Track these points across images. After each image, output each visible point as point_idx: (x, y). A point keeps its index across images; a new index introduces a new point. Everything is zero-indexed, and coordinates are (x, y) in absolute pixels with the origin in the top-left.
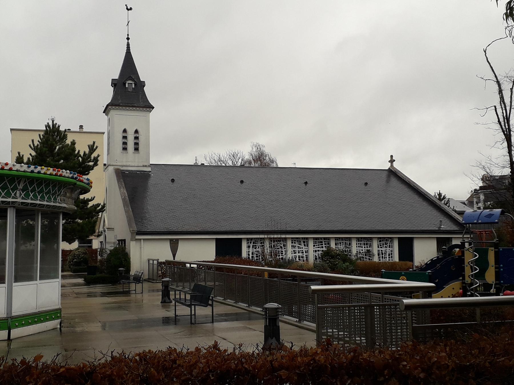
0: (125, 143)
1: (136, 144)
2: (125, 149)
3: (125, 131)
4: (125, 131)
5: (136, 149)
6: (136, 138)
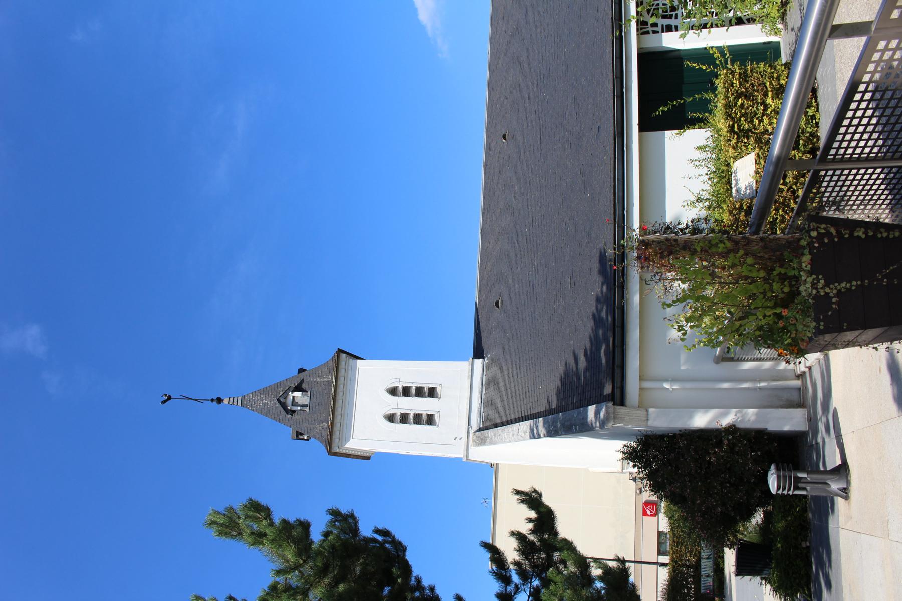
0: (418, 419)
1: (420, 392)
3: (391, 418)
4: (391, 418)
6: (406, 392)
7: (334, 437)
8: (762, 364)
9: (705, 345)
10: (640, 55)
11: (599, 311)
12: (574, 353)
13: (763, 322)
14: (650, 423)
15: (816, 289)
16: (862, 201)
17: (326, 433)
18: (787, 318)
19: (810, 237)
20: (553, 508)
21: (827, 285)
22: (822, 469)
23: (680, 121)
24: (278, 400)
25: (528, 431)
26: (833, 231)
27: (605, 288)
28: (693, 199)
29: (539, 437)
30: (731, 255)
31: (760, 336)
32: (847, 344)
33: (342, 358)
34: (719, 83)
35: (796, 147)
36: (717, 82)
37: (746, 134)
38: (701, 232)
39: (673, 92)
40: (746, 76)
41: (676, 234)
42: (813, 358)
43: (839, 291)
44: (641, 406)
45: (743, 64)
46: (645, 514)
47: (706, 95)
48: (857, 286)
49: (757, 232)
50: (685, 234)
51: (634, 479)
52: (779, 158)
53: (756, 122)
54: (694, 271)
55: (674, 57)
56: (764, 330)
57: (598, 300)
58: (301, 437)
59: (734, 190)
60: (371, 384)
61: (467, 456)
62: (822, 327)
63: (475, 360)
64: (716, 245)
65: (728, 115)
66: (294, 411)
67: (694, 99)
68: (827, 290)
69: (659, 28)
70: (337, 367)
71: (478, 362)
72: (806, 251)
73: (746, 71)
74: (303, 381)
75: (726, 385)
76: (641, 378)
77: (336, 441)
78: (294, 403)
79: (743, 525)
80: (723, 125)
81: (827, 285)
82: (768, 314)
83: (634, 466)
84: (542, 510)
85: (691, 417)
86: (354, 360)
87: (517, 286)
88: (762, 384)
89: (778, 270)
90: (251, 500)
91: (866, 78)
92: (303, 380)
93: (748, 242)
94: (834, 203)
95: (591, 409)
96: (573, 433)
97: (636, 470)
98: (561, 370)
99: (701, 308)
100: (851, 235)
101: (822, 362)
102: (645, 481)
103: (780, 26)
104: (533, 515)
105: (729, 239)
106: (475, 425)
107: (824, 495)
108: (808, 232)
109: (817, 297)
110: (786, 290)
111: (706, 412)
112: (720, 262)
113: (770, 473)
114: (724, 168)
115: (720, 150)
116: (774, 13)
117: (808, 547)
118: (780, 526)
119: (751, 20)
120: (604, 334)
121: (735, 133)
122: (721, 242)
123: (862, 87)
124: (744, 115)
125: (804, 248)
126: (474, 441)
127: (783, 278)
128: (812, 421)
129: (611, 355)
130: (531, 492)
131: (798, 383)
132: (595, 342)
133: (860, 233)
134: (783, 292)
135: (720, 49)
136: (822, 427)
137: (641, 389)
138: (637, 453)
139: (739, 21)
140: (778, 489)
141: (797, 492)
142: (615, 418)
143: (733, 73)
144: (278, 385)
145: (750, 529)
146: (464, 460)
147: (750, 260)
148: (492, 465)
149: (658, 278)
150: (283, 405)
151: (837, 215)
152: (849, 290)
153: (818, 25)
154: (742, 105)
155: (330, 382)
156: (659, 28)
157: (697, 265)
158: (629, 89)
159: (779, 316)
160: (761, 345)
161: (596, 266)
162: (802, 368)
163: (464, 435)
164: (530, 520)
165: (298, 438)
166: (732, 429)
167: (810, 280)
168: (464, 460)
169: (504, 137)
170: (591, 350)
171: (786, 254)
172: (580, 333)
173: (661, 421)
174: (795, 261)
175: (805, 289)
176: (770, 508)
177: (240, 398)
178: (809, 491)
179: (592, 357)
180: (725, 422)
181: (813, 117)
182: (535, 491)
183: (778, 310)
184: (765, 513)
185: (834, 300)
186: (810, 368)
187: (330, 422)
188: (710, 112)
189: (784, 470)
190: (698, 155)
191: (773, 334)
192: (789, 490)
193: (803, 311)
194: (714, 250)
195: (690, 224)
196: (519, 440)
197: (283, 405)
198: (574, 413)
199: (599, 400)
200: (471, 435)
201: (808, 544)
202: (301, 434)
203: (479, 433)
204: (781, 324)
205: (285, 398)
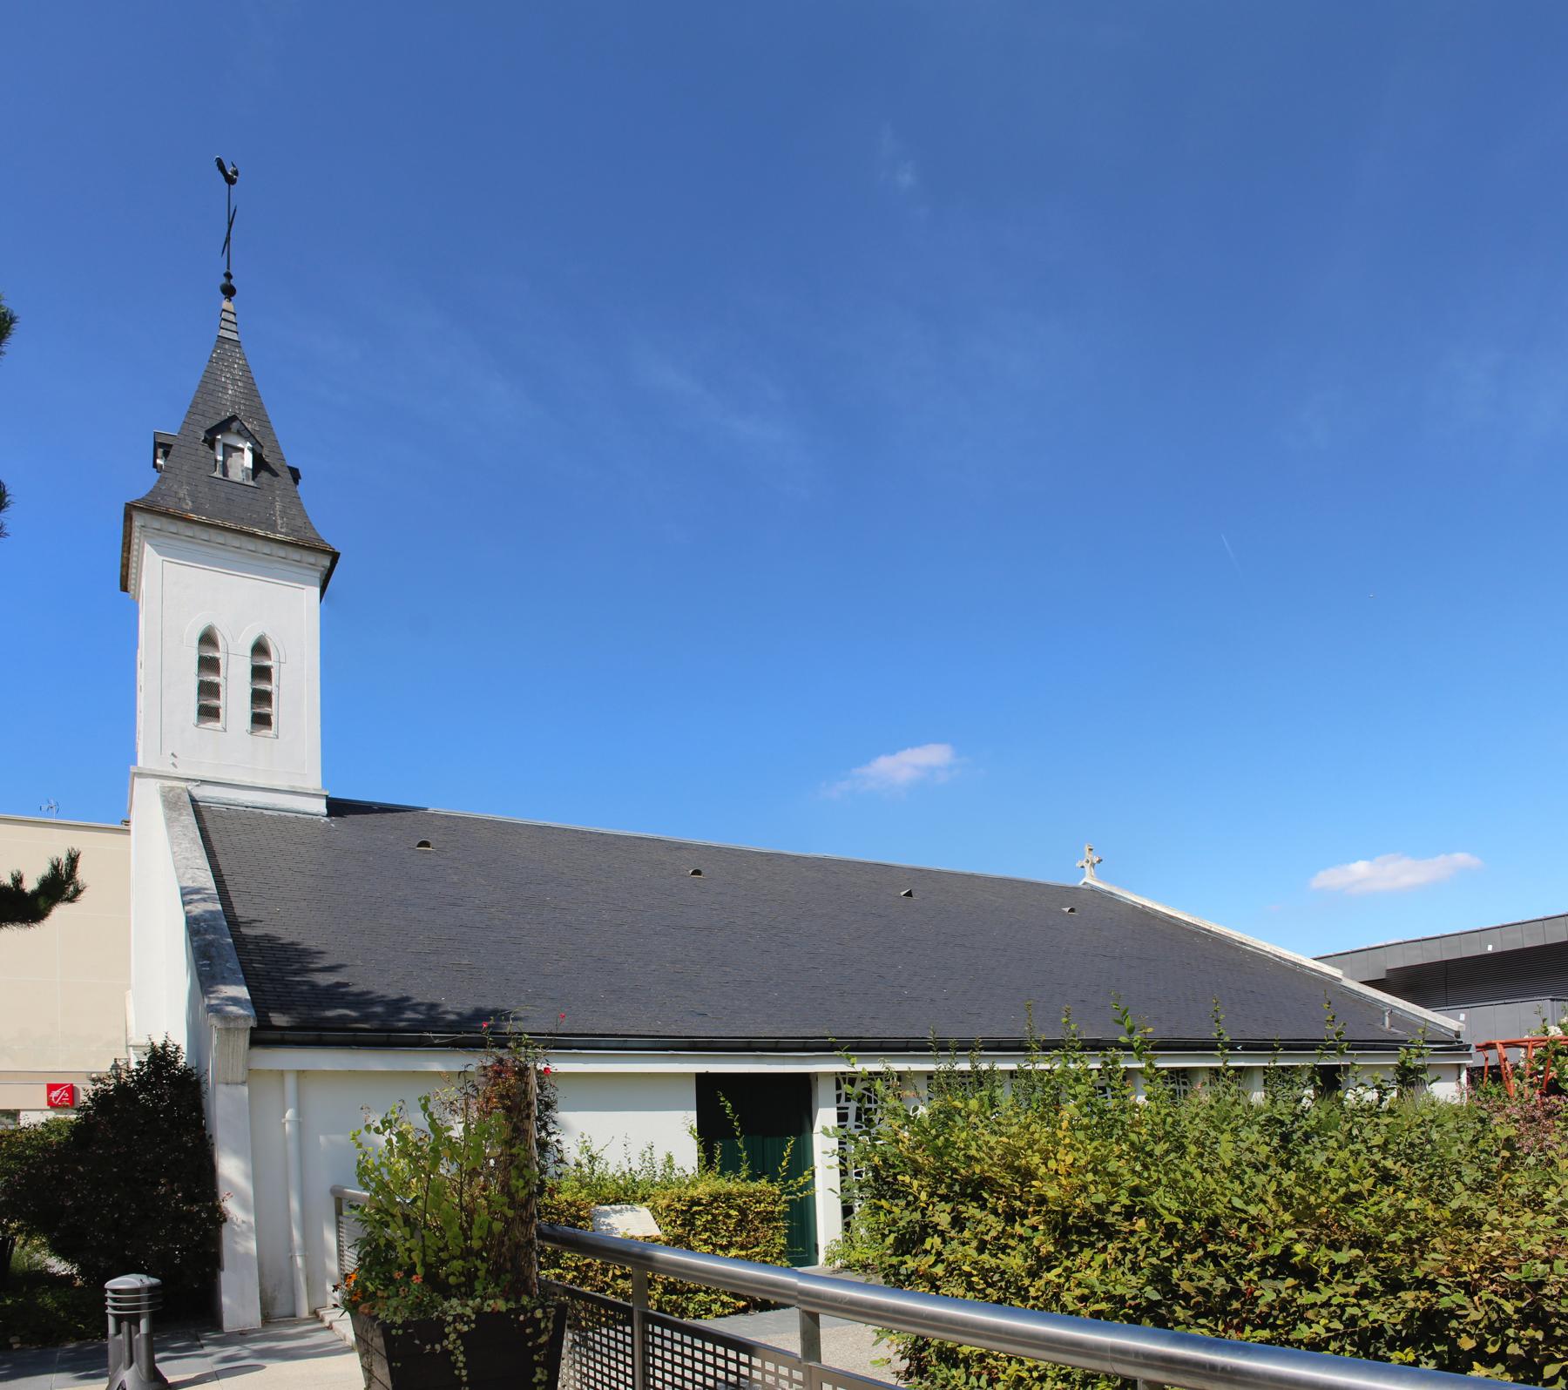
0: (208, 690)
1: (261, 697)
2: (208, 713)
3: (208, 639)
4: (208, 639)
5: (261, 720)
6: (261, 673)
7: (164, 520)
8: (334, 1254)
9: (359, 1162)
10: (806, 1078)
11: (414, 1008)
12: (341, 966)
13: (400, 1249)
14: (222, 1088)
15: (454, 1321)
16: (587, 1375)
17: (170, 504)
18: (408, 1284)
19: (535, 1309)
20: (47, 922)
21: (461, 1335)
22: (157, 1356)
23: (710, 1131)
24: (234, 418)
25: (196, 885)
26: (544, 1339)
27: (452, 1017)
28: (594, 1150)
29: (184, 904)
30: (505, 1199)
31: (378, 1245)
32: (368, 1370)
33: (327, 565)
34: (762, 1184)
35: (670, 1289)
36: (763, 1181)
37: (689, 1223)
38: (542, 1155)
39: (751, 1122)
40: (769, 1221)
41: (539, 1119)
42: (345, 1327)
43: (452, 1353)
44: (252, 1075)
45: (786, 1216)
46: (51, 1088)
47: (745, 1167)
48: (460, 1376)
49: (541, 1235)
50: (539, 1131)
51: (115, 1067)
52: (650, 1259)
53: (705, 1236)
54: (480, 1145)
55: (801, 1122)
56: (386, 1251)
57: (433, 1006)
58: (160, 451)
59: (606, 1208)
60: (277, 609)
61: (141, 775)
62: (394, 1332)
63: (324, 802)
64: (521, 1176)
65: (715, 1198)
66: (212, 446)
67: (740, 1151)
68: (453, 1337)
69: (843, 1103)
70: (303, 547)
71: (320, 807)
72: (512, 1305)
73: (776, 1220)
74: (275, 474)
75: (295, 1205)
76: (300, 1074)
77: (157, 522)
78: (229, 450)
79: (43, 1244)
80: (702, 1191)
81: (461, 1335)
82: (413, 1255)
83: (139, 1063)
84: (42, 902)
85: (236, 1152)
86: (318, 582)
87: (455, 879)
88: (299, 1261)
89: (483, 1267)
90: (12, 320)
91: (756, 1362)
92: (276, 475)
93: (526, 1223)
94: (586, 1338)
95: (242, 992)
96: (196, 962)
97: (134, 1066)
98: (310, 943)
99: (425, 1153)
100: (538, 1364)
101: (341, 1345)
102: (113, 1081)
103: (838, 1263)
104: (30, 885)
105: (531, 1195)
106: (201, 792)
107: (111, 1361)
108: (542, 1306)
109: (441, 1322)
110: (452, 1280)
111: (247, 1177)
112: (494, 1189)
113: (144, 1277)
114: (639, 1195)
115: (666, 1188)
116: (855, 1256)
117: (10, 1346)
118: (48, 1301)
119: (847, 1225)
120: (375, 1015)
121: (690, 1208)
122: (527, 1183)
123: (744, 1358)
124: (715, 1219)
125: (518, 1301)
126: (172, 789)
127: (471, 1276)
128: (242, 1337)
129: (341, 1024)
130: (76, 884)
131: (304, 1311)
132: (362, 1001)
133: (540, 1375)
134: (448, 1276)
135: (810, 1185)
136: (231, 1351)
137: (282, 1073)
138: (165, 1067)
139: (847, 1211)
140: (115, 1291)
141: (111, 1321)
142: (228, 1030)
143: (775, 1203)
144: (265, 422)
145: (37, 1256)
146: (133, 769)
147: (498, 1226)
148: (127, 822)
149: (470, 1090)
150: (224, 426)
151: (567, 1344)
152: (454, 1365)
153: (817, 1295)
154: (729, 1216)
155: (272, 527)
156: (843, 1103)
157: (492, 1151)
158: (759, 1060)
159: (411, 1271)
160: (362, 1248)
161: (489, 1004)
162: (330, 1315)
163: (180, 772)
164: (18, 880)
165: (157, 445)
166: (217, 1218)
167: (468, 1311)
168: (133, 769)
169: (697, 872)
170: (347, 994)
171: (509, 1276)
172: (376, 975)
173: (225, 1107)
174: (497, 1290)
175: (454, 1306)
176: (79, 1282)
177: (234, 337)
178: (116, 1340)
179: (335, 995)
180: (231, 1206)
181: (708, 1311)
182: (78, 892)
183: (419, 1269)
184: (70, 1277)
185: (438, 1347)
186: (330, 1328)
187: (194, 517)
188: (721, 1173)
189: (150, 1298)
190: (660, 1156)
191: (382, 1265)
192: (115, 1308)
193: (420, 1304)
194: (514, 1173)
195: (554, 1138)
196: (177, 869)
197: (224, 426)
198: (233, 964)
199: (259, 1003)
200: (183, 784)
201: (16, 1346)
202: (166, 454)
203: (187, 799)
204: (398, 1275)
205: (239, 433)
